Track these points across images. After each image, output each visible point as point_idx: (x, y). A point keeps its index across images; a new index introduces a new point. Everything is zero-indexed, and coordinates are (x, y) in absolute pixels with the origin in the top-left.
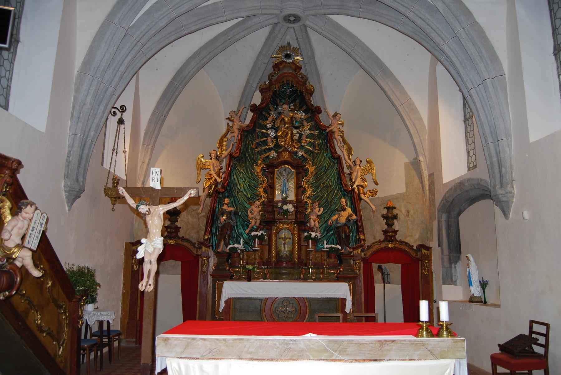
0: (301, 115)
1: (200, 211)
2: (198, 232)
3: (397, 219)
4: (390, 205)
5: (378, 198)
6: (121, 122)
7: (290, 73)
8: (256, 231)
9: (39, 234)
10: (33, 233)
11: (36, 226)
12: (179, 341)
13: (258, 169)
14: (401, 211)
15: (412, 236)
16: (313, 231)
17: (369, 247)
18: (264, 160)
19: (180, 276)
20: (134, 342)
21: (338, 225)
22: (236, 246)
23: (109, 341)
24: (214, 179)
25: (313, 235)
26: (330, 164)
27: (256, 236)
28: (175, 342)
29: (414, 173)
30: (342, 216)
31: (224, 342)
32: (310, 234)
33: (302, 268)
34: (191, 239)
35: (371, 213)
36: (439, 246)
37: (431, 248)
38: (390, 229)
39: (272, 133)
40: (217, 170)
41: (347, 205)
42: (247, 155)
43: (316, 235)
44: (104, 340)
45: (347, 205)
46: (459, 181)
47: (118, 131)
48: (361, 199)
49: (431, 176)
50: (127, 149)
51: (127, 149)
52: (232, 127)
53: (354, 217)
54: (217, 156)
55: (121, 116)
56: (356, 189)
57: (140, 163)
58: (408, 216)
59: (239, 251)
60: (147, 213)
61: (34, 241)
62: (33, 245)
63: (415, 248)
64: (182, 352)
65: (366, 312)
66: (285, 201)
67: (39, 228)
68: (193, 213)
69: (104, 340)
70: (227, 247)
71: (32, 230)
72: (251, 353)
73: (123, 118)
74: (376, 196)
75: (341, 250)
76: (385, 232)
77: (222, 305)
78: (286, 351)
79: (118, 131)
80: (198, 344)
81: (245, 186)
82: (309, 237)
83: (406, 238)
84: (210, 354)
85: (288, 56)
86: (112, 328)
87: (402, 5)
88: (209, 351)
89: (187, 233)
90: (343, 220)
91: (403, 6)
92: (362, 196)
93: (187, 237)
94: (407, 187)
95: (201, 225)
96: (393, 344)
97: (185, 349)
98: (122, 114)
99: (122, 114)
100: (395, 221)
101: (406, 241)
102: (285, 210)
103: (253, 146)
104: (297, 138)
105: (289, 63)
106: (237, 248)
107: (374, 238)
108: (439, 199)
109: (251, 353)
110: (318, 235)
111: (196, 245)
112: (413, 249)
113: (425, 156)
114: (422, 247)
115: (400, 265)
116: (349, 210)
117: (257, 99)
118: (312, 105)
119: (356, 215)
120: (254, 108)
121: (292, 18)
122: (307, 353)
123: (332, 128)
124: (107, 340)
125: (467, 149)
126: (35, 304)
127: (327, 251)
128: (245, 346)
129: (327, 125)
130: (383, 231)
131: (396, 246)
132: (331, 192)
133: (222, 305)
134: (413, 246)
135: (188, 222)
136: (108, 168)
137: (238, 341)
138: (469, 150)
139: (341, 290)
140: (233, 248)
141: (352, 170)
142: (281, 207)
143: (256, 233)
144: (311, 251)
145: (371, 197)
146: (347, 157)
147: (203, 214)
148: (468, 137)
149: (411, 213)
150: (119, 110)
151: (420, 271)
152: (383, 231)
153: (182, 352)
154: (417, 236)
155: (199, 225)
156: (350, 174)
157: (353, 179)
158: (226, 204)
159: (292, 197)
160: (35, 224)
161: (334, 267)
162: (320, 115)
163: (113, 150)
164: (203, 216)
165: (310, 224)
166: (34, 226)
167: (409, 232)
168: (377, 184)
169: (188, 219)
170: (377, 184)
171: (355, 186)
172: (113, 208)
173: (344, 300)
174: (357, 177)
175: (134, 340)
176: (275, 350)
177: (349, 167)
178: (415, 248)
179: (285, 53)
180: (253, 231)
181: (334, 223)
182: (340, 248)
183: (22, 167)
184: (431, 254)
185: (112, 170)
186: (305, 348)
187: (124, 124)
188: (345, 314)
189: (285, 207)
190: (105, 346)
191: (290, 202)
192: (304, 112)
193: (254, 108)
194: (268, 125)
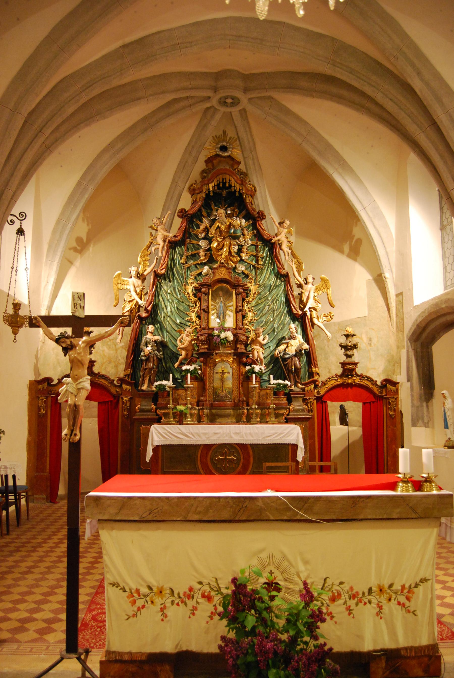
0: (240, 222)
1: (118, 341)
2: (116, 366)
3: (357, 348)
4: (350, 330)
5: (334, 323)
6: (20, 232)
7: (226, 169)
8: (188, 364)
12: (113, 501)
13: (190, 289)
14: (361, 338)
15: (375, 369)
16: (257, 364)
17: (324, 384)
18: (195, 278)
19: (97, 419)
20: (44, 499)
21: (287, 356)
22: (164, 382)
23: (16, 499)
24: (135, 302)
25: (257, 368)
26: (276, 283)
27: (187, 371)
28: (109, 502)
29: (377, 293)
30: (291, 345)
31: (167, 501)
32: (253, 368)
33: (244, 409)
34: (108, 375)
35: (326, 342)
36: (408, 380)
37: (398, 383)
38: (349, 360)
39: (203, 243)
40: (138, 291)
41: (296, 332)
42: (174, 270)
43: (260, 369)
44: (10, 497)
45: (296, 332)
46: (434, 302)
47: (17, 243)
48: (313, 324)
49: (399, 295)
50: (29, 267)
51: (29, 267)
52: (155, 238)
53: (306, 346)
54: (138, 273)
55: (21, 226)
56: (308, 313)
57: (43, 285)
58: (370, 344)
59: (168, 389)
60: (69, 347)
63: (379, 383)
64: (117, 514)
65: (321, 460)
66: (223, 329)
68: (109, 343)
69: (13, 497)
70: (152, 384)
72: (199, 513)
73: (22, 227)
74: (332, 321)
75: (291, 387)
76: (343, 364)
77: (150, 453)
78: (242, 510)
79: (17, 243)
81: (173, 310)
82: (252, 371)
83: (367, 372)
84: (151, 516)
85: (224, 149)
86: (18, 483)
87: (368, 83)
88: (149, 512)
89: (103, 367)
90: (292, 351)
91: (371, 85)
92: (315, 321)
93: (103, 372)
94: (369, 310)
95: (120, 358)
96: (368, 500)
97: (120, 510)
98: (21, 223)
99: (21, 223)
100: (355, 350)
101: (368, 375)
102: (223, 339)
103: (182, 261)
104: (236, 251)
105: (225, 157)
106: (164, 386)
107: (329, 372)
108: (410, 323)
109: (199, 513)
110: (263, 369)
111: (115, 382)
112: (377, 385)
113: (392, 272)
114: (388, 382)
115: (361, 404)
116: (300, 338)
117: (186, 202)
118: (254, 210)
119: (308, 344)
120: (183, 214)
121: (229, 101)
122: (267, 512)
123: (278, 238)
124: (13, 497)
125: (444, 264)
127: (274, 388)
128: (192, 505)
129: (272, 234)
130: (341, 363)
131: (356, 382)
132: (277, 316)
133: (150, 453)
134: (376, 381)
135: (104, 354)
136: (6, 290)
137: (183, 500)
138: (446, 264)
139: (292, 434)
140: (161, 385)
141: (302, 288)
142: (218, 336)
143: (188, 367)
144: (255, 387)
145: (326, 322)
146: (296, 274)
147: (122, 344)
148: (445, 249)
149: (374, 341)
150: (17, 218)
151: (385, 411)
152: (341, 363)
153: (117, 514)
154: (381, 368)
155: (117, 358)
156: (301, 295)
157: (304, 299)
158: (151, 333)
159: (230, 322)
161: (277, 408)
162: (263, 222)
163: (12, 268)
164: (122, 347)
165: (253, 356)
167: (373, 366)
168: (332, 306)
169: (103, 351)
170: (332, 306)
171: (307, 309)
172: (15, 339)
173: (295, 447)
174: (308, 298)
175: (44, 496)
176: (229, 509)
177: (300, 286)
178: (379, 383)
179: (221, 144)
180: (184, 364)
181: (282, 354)
182: (289, 383)
184: (397, 390)
185: (11, 293)
186: (264, 506)
187: (24, 235)
188: (297, 462)
189: (223, 335)
190: (12, 504)
191: (229, 329)
192: (244, 218)
193: (183, 214)
194: (200, 235)
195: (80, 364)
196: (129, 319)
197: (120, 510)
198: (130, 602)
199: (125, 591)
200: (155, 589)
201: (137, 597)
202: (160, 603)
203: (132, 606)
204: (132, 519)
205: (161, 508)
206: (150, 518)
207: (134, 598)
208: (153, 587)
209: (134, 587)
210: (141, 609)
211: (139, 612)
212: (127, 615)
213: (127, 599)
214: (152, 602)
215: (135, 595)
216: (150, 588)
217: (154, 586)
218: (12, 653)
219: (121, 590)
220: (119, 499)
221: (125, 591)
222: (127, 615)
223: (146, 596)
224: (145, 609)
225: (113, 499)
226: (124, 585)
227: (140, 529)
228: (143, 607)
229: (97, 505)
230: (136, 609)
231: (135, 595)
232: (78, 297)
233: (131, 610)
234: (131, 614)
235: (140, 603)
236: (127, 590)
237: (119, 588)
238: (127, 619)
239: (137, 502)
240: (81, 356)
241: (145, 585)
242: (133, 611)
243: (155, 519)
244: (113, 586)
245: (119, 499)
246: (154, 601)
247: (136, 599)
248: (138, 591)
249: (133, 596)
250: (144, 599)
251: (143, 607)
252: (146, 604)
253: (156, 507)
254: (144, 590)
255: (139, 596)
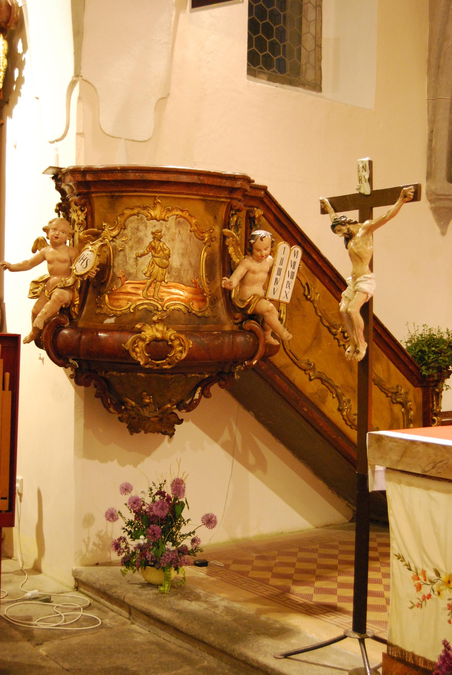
9: (292, 278)
10: (280, 278)
11: (283, 267)
12: (395, 444)
28: (391, 444)
61: (284, 289)
62: (283, 294)
64: (398, 462)
67: (290, 269)
71: (279, 274)
80: (418, 452)
126: (336, 383)
130: (58, 176)
160: (281, 264)
166: (281, 267)
183: (267, 188)
195: (357, 258)
196: (413, 190)
197: (402, 456)
198: (415, 585)
199: (410, 569)
200: (443, 575)
201: (423, 581)
202: (447, 597)
203: (417, 591)
204: (414, 471)
205: (446, 461)
206: (433, 473)
207: (419, 581)
208: (440, 573)
209: (420, 566)
210: (427, 600)
211: (424, 602)
212: (412, 603)
213: (412, 581)
214: (439, 593)
215: (421, 577)
216: (438, 573)
217: (442, 572)
218: (338, 624)
219: (406, 567)
220: (401, 441)
221: (410, 569)
222: (412, 603)
223: (432, 582)
224: (430, 599)
225: (395, 442)
226: (410, 560)
227: (428, 488)
228: (429, 596)
229: (379, 446)
230: (421, 597)
231: (421, 577)
232: (363, 167)
233: (416, 597)
234: (416, 602)
235: (426, 590)
236: (413, 569)
237: (404, 563)
238: (411, 608)
239: (420, 449)
240: (358, 248)
241: (432, 567)
242: (418, 599)
243: (439, 476)
244: (399, 558)
245: (401, 441)
246: (441, 593)
247: (422, 583)
248: (424, 572)
249: (419, 579)
250: (431, 586)
251: (429, 596)
252: (432, 593)
253: (440, 460)
254: (431, 574)
255: (425, 580)
